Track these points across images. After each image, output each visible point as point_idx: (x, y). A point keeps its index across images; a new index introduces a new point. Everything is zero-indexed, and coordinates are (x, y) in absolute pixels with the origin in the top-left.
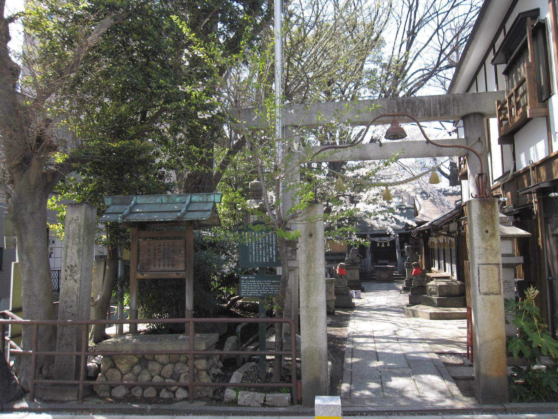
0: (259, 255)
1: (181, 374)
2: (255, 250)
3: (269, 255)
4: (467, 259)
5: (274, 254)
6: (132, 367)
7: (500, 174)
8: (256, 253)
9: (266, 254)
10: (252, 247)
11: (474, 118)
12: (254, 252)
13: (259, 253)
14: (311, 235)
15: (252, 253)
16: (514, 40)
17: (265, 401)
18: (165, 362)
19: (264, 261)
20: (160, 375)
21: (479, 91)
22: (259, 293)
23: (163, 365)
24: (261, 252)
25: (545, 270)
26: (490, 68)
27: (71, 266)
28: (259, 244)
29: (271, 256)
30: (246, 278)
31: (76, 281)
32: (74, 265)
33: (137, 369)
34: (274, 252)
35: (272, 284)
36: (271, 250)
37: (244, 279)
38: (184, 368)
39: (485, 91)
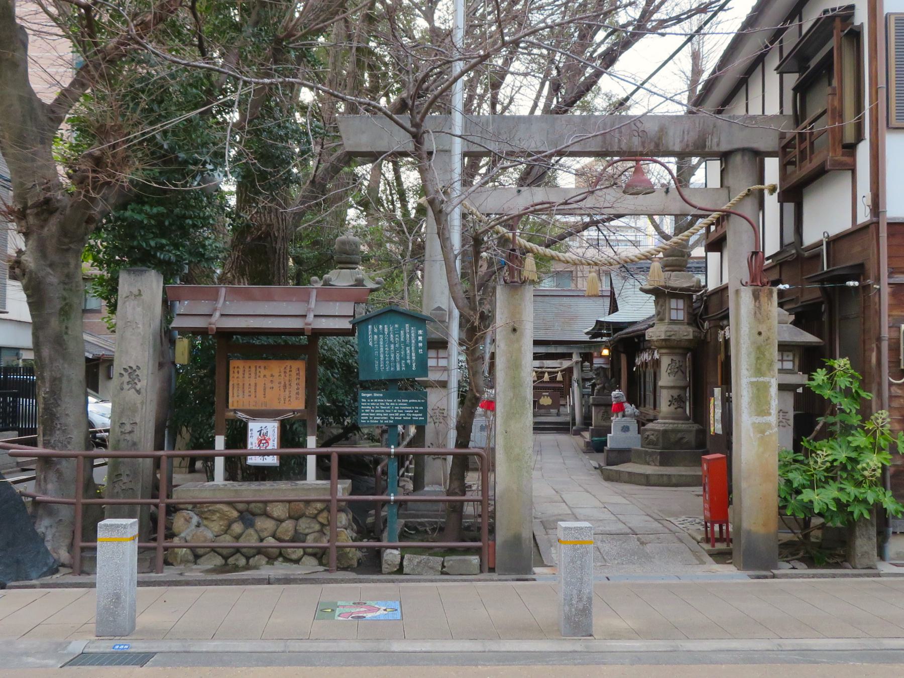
0: (390, 361)
1: (307, 535)
2: (384, 353)
3: (406, 360)
5: (414, 358)
6: (229, 526)
8: (385, 357)
9: (401, 359)
10: (379, 348)
11: (743, 156)
12: (382, 356)
13: (390, 357)
15: (379, 357)
16: (815, 54)
17: (443, 566)
18: (283, 517)
19: (398, 369)
20: (274, 537)
21: (751, 113)
22: (389, 419)
23: (280, 521)
24: (392, 355)
25: (879, 313)
26: (772, 79)
27: (131, 367)
28: (390, 343)
29: (409, 361)
30: (368, 395)
31: (138, 392)
32: (135, 368)
33: (237, 528)
34: (413, 354)
35: (410, 404)
36: (408, 352)
37: (365, 398)
38: (313, 525)
39: (761, 113)
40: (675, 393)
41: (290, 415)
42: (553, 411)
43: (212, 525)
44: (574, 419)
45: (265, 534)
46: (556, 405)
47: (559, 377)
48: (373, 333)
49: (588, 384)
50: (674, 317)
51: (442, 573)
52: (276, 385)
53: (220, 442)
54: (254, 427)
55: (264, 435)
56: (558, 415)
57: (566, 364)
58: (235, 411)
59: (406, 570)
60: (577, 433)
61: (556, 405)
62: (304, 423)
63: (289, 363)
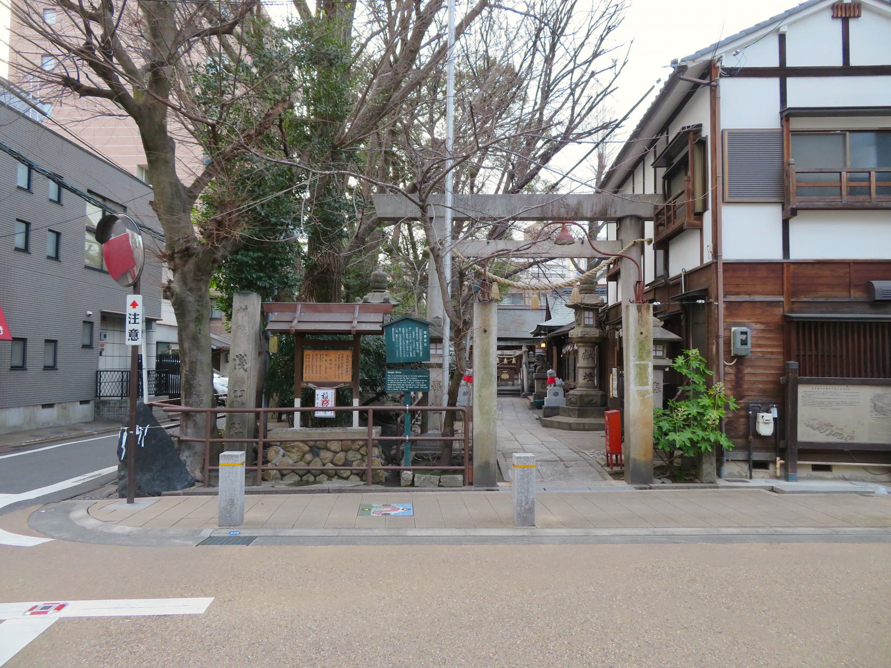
4: (472, 421)
6: (303, 456)
7: (653, 279)
14: (485, 331)
17: (440, 482)
21: (636, 192)
23: (336, 453)
25: (717, 320)
31: (245, 370)
33: (309, 457)
40: (588, 371)
41: (342, 385)
42: (510, 383)
43: (292, 455)
44: (523, 388)
45: (326, 461)
46: (512, 379)
47: (514, 361)
48: (395, 333)
49: (532, 365)
50: (587, 323)
51: (439, 486)
52: (333, 366)
53: (297, 402)
54: (319, 393)
55: (325, 397)
56: (513, 385)
57: (518, 353)
58: (307, 382)
59: (416, 484)
60: (525, 397)
61: (512, 379)
62: (351, 390)
63: (341, 352)
